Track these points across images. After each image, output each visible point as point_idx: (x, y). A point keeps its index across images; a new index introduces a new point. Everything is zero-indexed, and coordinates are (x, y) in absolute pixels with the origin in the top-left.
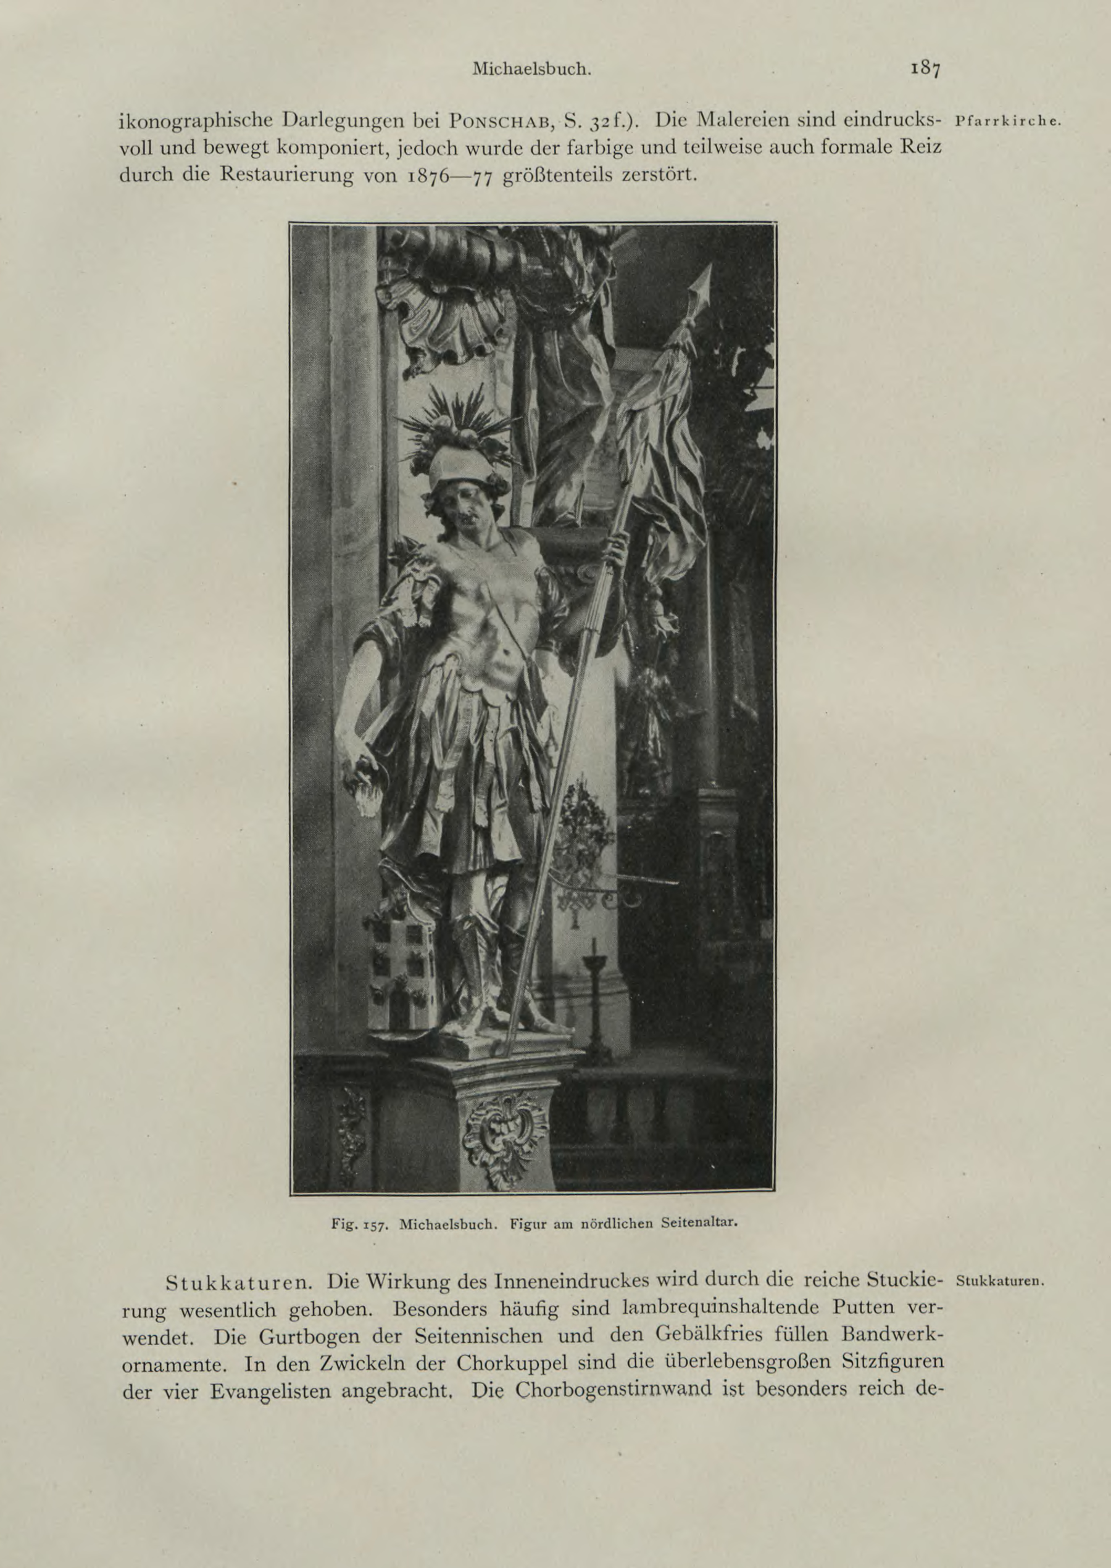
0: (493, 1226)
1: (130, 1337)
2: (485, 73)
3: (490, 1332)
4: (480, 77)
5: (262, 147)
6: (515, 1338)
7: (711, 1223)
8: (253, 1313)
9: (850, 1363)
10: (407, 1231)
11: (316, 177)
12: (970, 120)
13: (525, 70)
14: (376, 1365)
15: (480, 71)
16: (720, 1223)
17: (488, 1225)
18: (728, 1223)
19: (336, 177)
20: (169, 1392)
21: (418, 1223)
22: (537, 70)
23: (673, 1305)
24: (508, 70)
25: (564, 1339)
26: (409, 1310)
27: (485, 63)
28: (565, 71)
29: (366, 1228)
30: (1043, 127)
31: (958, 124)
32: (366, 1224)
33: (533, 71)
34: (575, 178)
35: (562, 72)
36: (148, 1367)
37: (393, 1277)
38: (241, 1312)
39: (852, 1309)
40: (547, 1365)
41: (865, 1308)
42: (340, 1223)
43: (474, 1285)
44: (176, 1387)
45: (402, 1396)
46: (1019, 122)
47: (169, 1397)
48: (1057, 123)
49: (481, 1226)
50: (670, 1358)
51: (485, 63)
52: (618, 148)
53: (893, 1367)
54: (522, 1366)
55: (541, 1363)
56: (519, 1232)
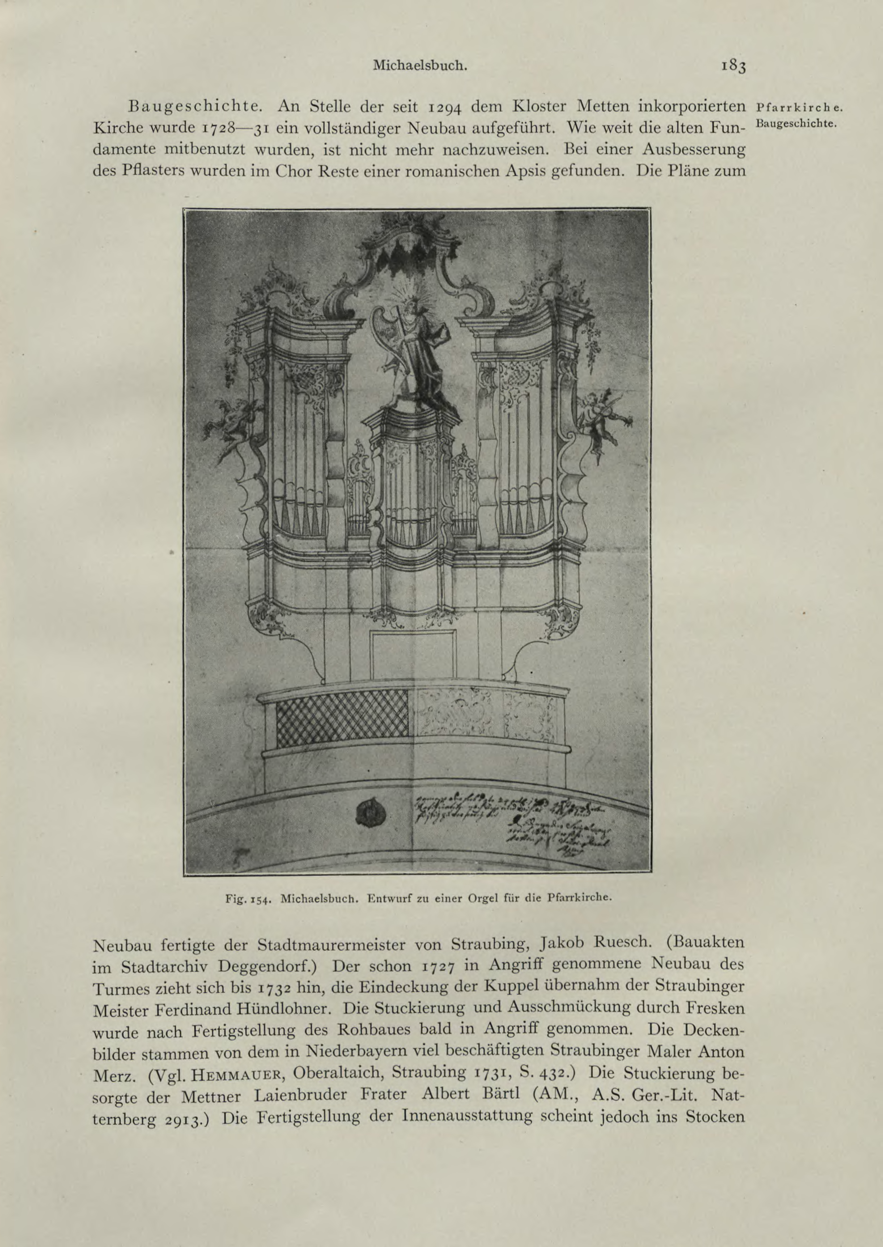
0: (355, 901)
2: (383, 69)
4: (379, 71)
6: (560, 1117)
11: (716, 151)
12: (768, 107)
13: (415, 66)
15: (379, 67)
17: (351, 899)
18: (565, 899)
19: (732, 150)
20: (418, 1050)
21: (295, 897)
22: (420, 66)
24: (401, 66)
26: (577, 149)
28: (446, 67)
29: (253, 902)
31: (759, 110)
32: (253, 898)
34: (143, 151)
35: (444, 68)
40: (522, 987)
42: (232, 899)
44: (423, 1046)
46: (808, 109)
47: (417, 1054)
49: (345, 899)
52: (381, 129)
54: (502, 988)
55: (517, 985)
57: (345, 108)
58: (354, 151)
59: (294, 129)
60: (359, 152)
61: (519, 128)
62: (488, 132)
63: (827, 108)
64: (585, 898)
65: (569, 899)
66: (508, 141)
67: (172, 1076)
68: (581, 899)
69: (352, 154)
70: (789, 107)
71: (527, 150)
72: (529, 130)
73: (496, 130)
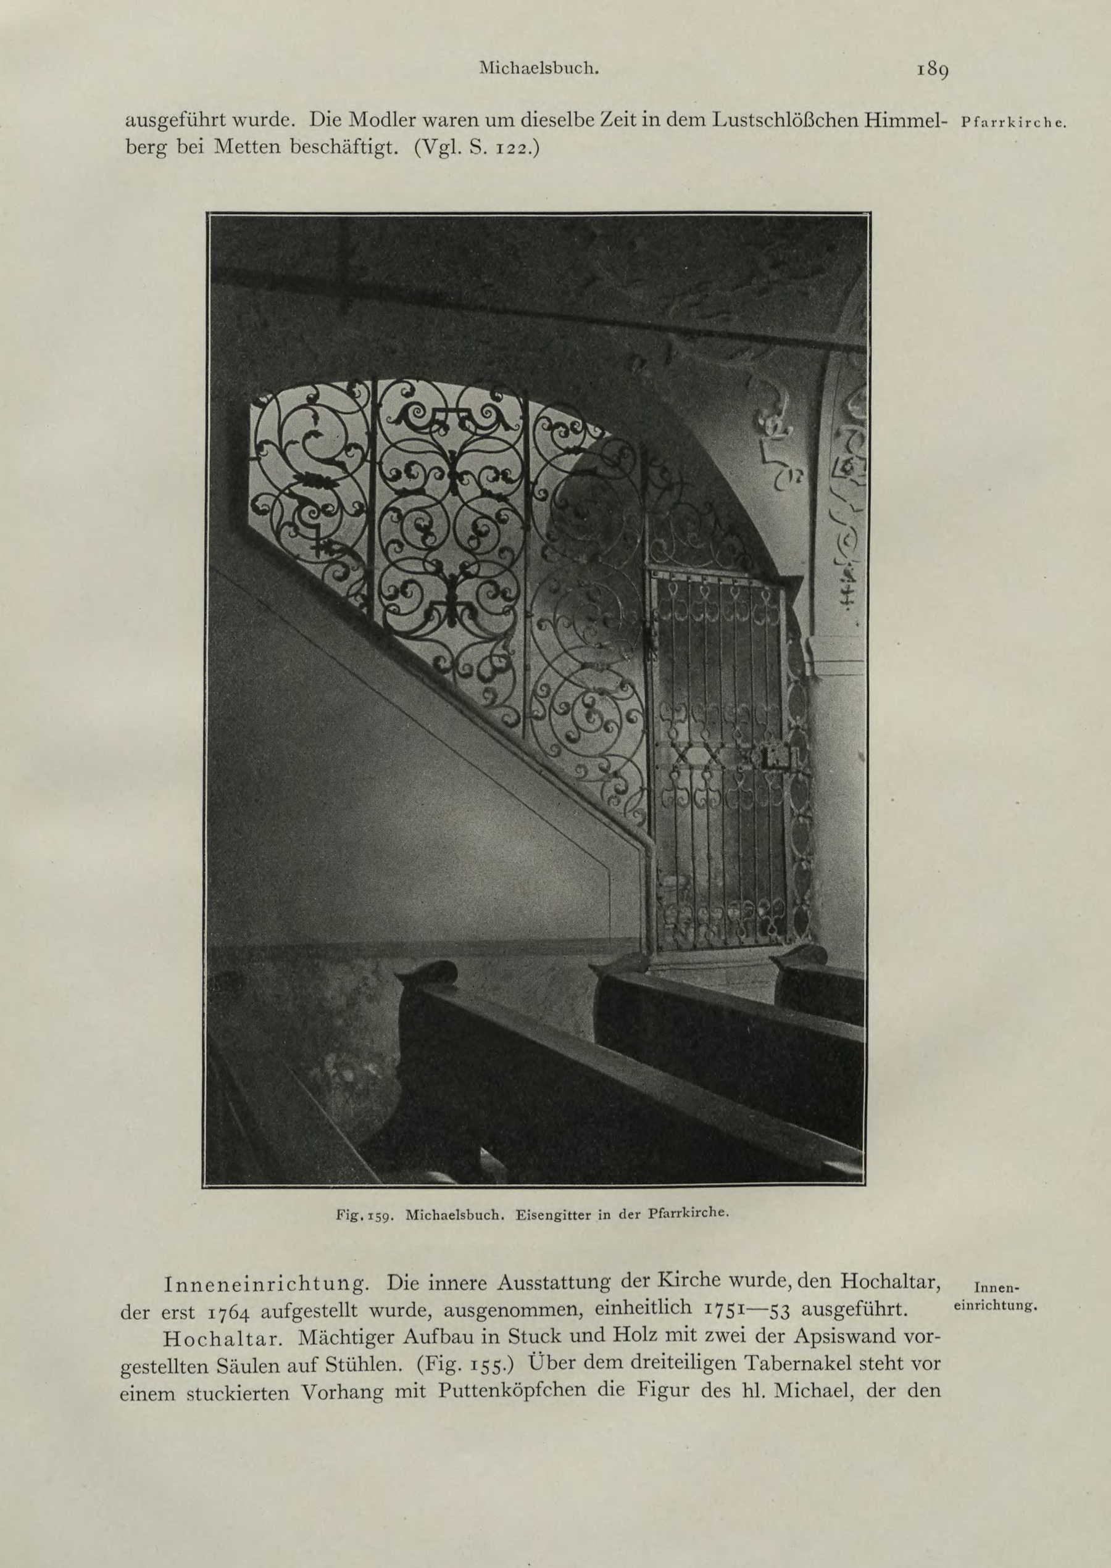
0: (500, 1217)
1: (854, 1334)
3: (836, 1332)
5: (385, 147)
8: (669, 1310)
10: (413, 1222)
14: (834, 1365)
17: (495, 1216)
18: (670, 1215)
22: (546, 69)
24: (515, 68)
25: (575, 1338)
27: (492, 63)
29: (371, 1218)
32: (371, 1214)
33: (540, 70)
36: (807, 1365)
37: (680, 1275)
38: (657, 1309)
39: (458, 1393)
41: (470, 1392)
45: (332, 1398)
46: (1024, 124)
49: (487, 1216)
50: (351, 1361)
51: (492, 63)
56: (344, 1222)
63: (1048, 124)
64: (695, 1214)
65: (676, 1215)
66: (851, 1324)
67: (444, 147)
68: (690, 1214)
73: (290, 1313)
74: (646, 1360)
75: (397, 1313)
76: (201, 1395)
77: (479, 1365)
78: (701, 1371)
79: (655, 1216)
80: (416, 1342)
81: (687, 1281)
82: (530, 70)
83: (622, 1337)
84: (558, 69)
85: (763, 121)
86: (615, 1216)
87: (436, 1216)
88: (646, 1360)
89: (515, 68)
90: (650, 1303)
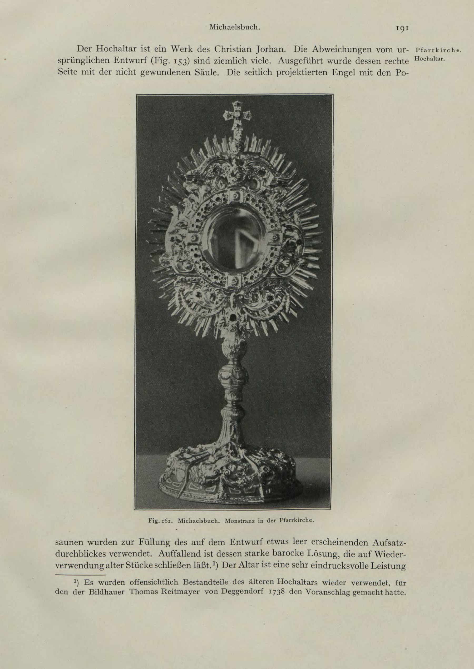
4: (213, 30)
6: (98, 61)
7: (433, 59)
9: (129, 566)
12: (422, 50)
15: (213, 28)
16: (437, 59)
17: (216, 521)
18: (289, 521)
22: (237, 27)
23: (283, 71)
24: (224, 27)
27: (215, 25)
29: (163, 522)
30: (453, 53)
31: (417, 52)
32: (163, 520)
42: (152, 520)
43: (182, 544)
46: (443, 51)
48: (460, 51)
49: (213, 522)
53: (100, 568)
57: (304, 50)
58: (118, 72)
59: (207, 61)
60: (121, 73)
61: (306, 61)
62: (337, 63)
63: (453, 51)
64: (300, 521)
65: (291, 521)
68: (297, 521)
69: (117, 74)
70: (433, 50)
71: (295, 565)
72: (311, 62)
74: (329, 565)
75: (66, 555)
76: (390, 567)
77: (177, 61)
78: (401, 570)
79: (283, 521)
80: (283, 63)
81: (68, 555)
82: (231, 28)
83: (100, 50)
84: (243, 28)
85: (158, 565)
86: (265, 522)
87: (190, 521)
88: (329, 565)
89: (225, 27)
90: (254, 70)
